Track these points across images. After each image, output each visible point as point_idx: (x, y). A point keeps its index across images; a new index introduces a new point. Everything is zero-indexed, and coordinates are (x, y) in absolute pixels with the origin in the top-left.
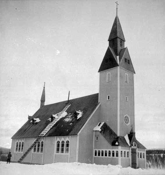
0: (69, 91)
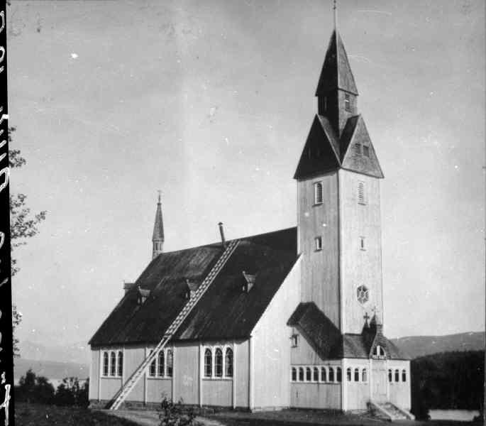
0: (220, 224)
